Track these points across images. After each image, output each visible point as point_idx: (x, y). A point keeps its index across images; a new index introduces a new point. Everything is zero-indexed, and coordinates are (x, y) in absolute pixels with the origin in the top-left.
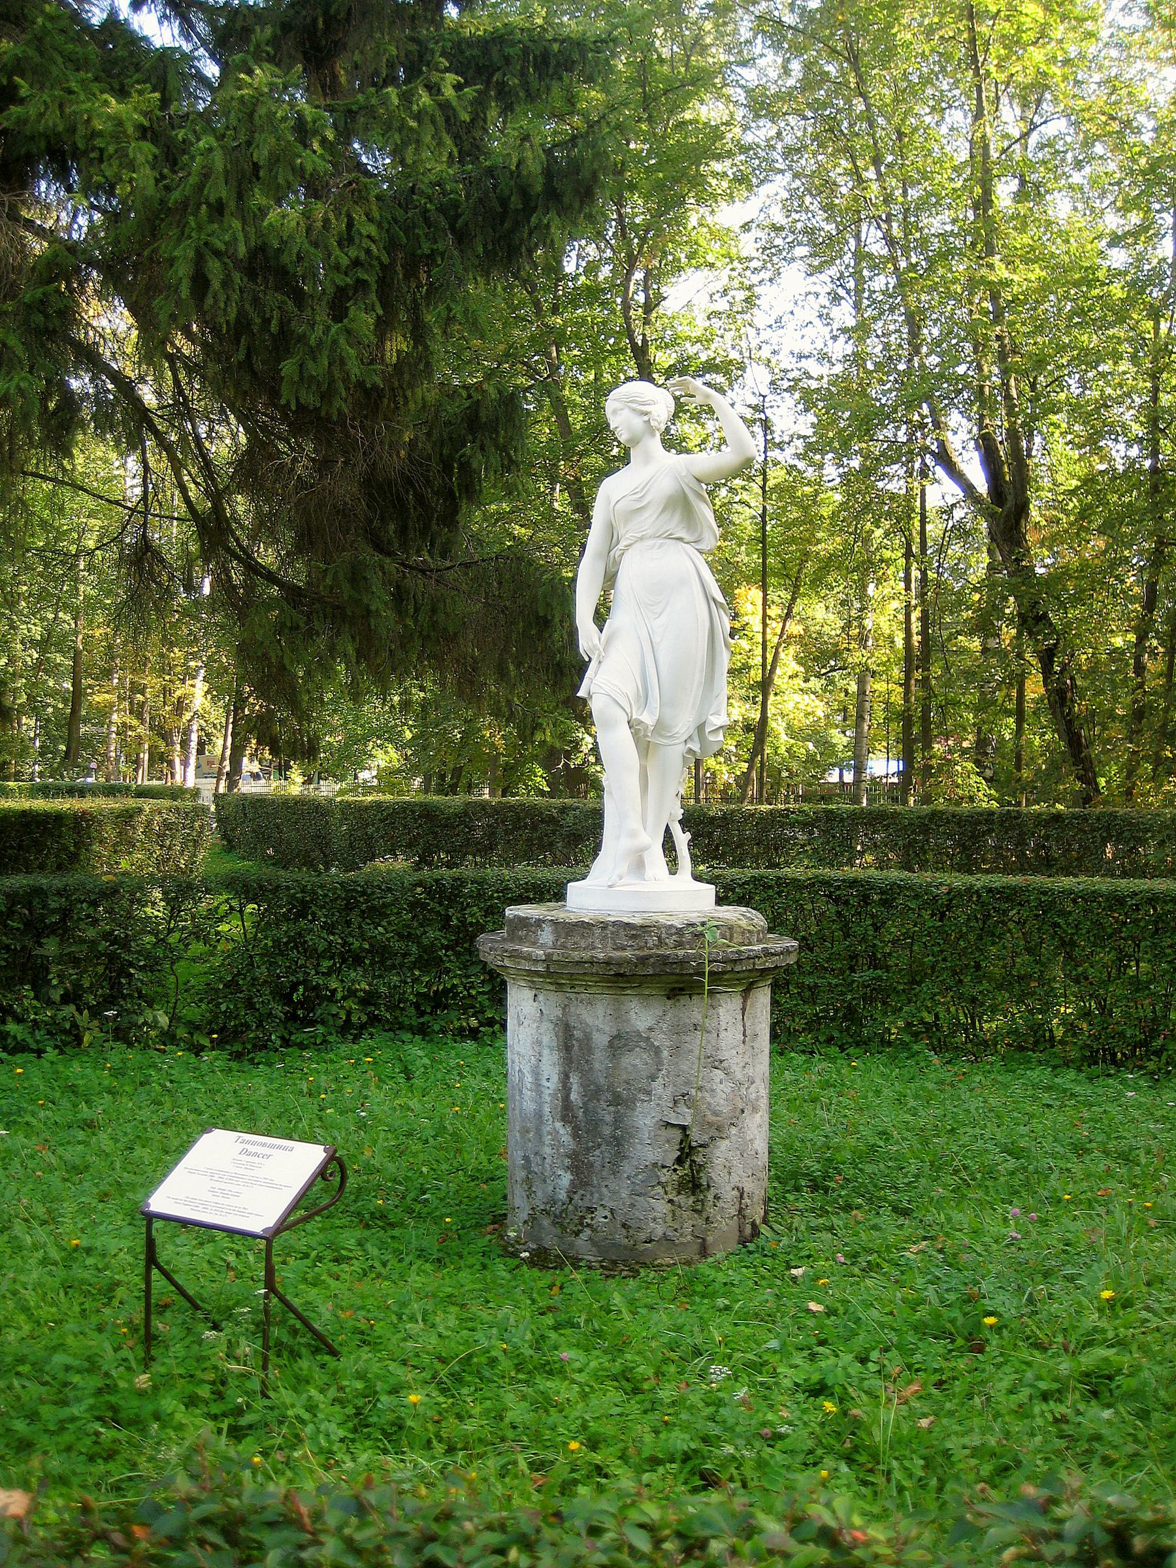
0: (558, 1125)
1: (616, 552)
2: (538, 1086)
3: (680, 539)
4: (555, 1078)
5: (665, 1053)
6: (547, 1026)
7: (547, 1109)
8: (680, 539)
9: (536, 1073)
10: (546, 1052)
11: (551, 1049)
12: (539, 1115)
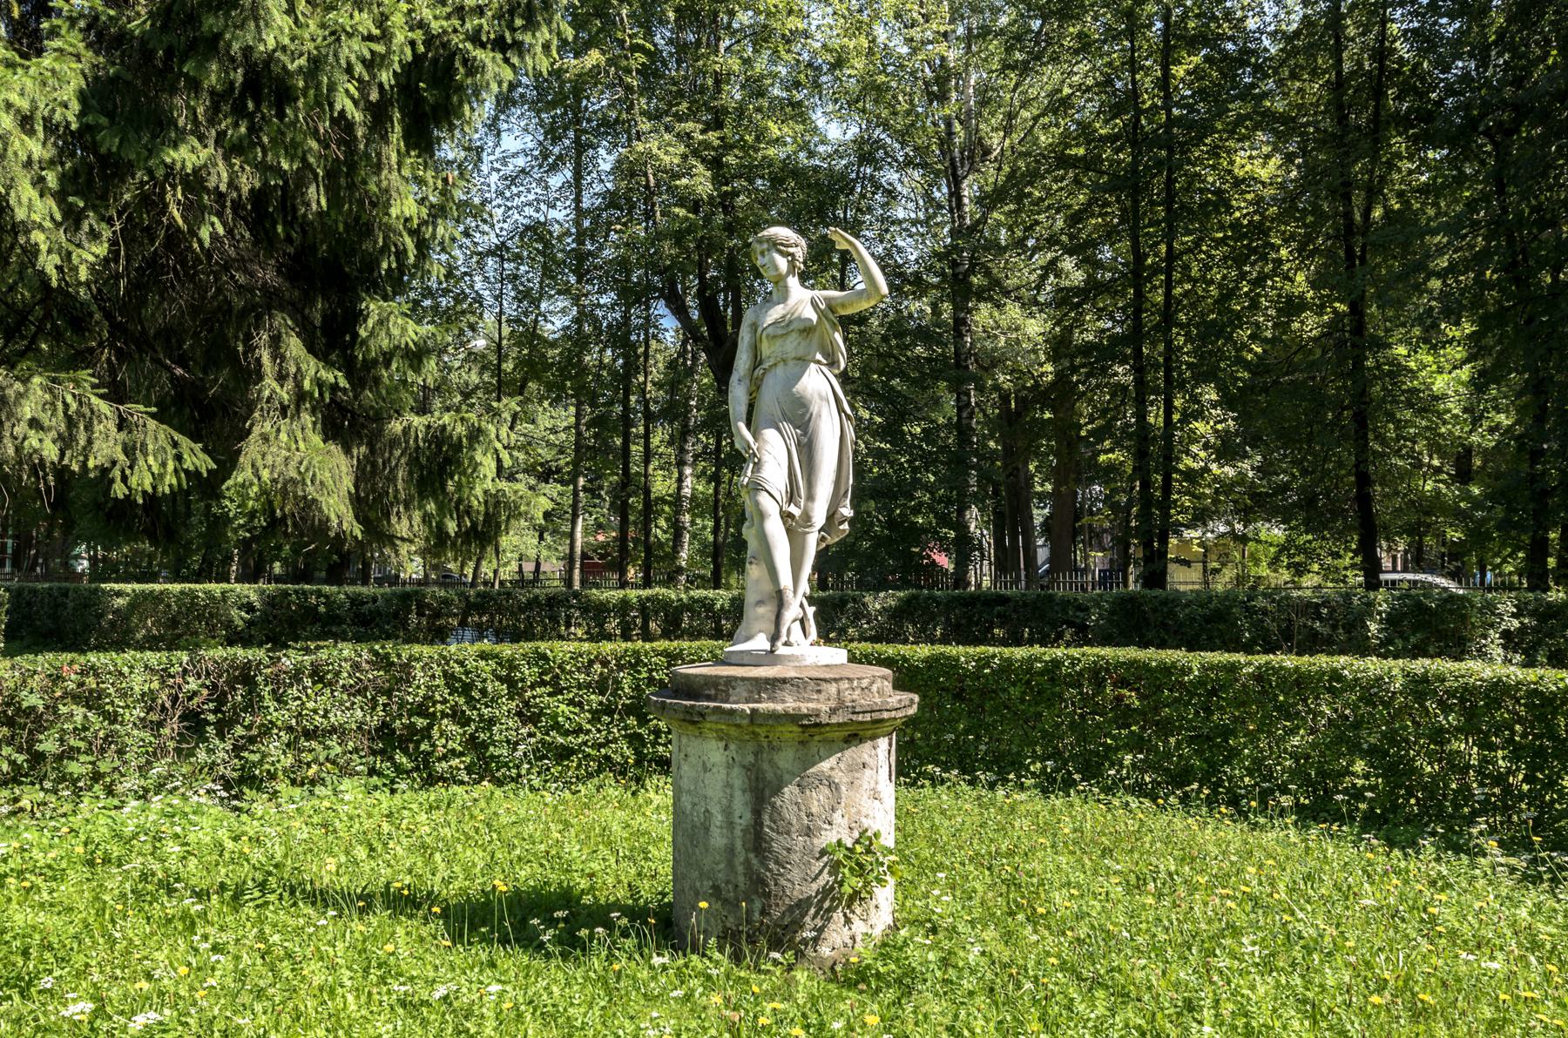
0: (752, 856)
1: (759, 372)
2: (730, 825)
4: (748, 816)
5: (843, 788)
6: (736, 770)
7: (739, 844)
9: (727, 812)
10: (738, 793)
11: (744, 791)
12: (730, 850)
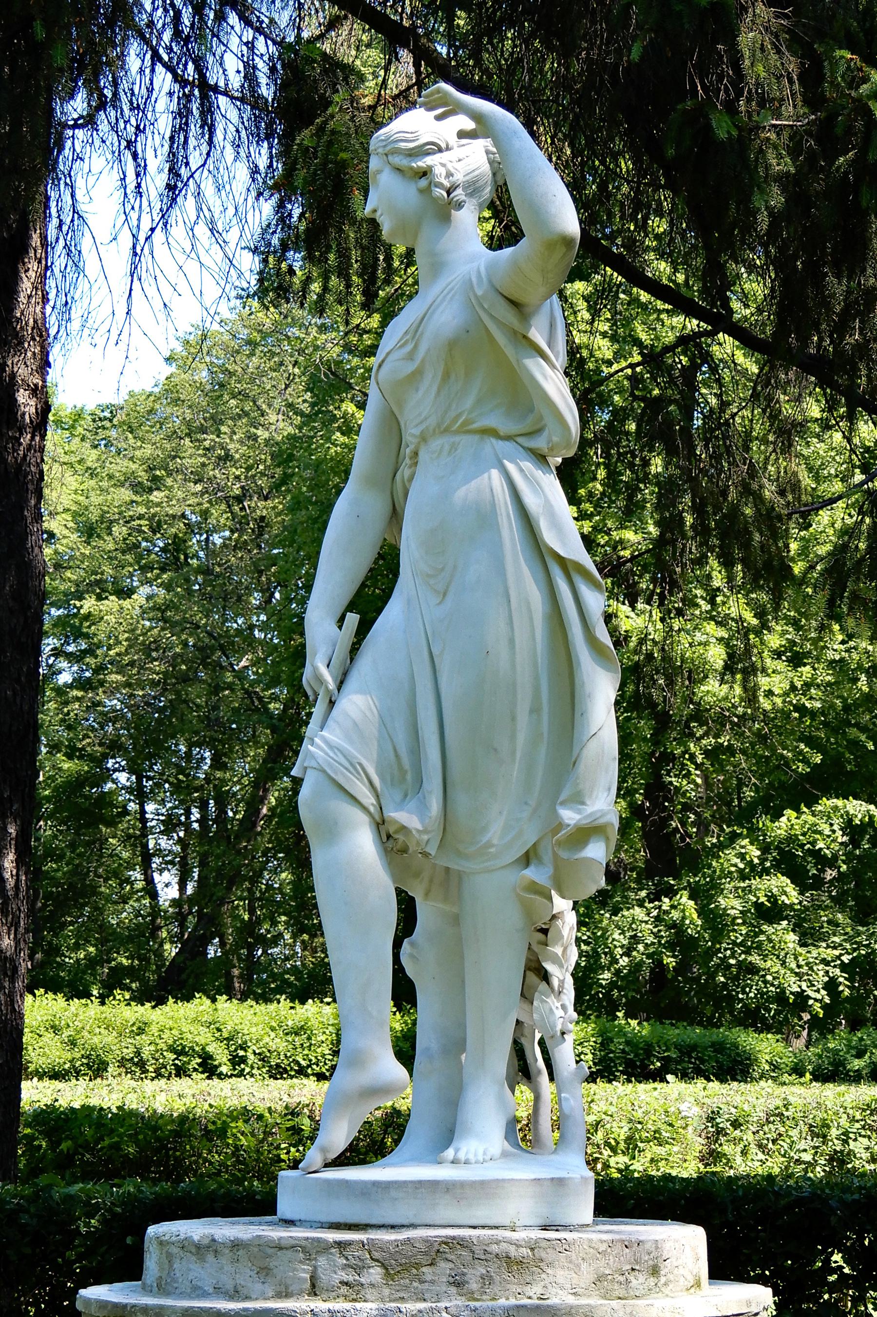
3: (492, 432)
8: (492, 432)
